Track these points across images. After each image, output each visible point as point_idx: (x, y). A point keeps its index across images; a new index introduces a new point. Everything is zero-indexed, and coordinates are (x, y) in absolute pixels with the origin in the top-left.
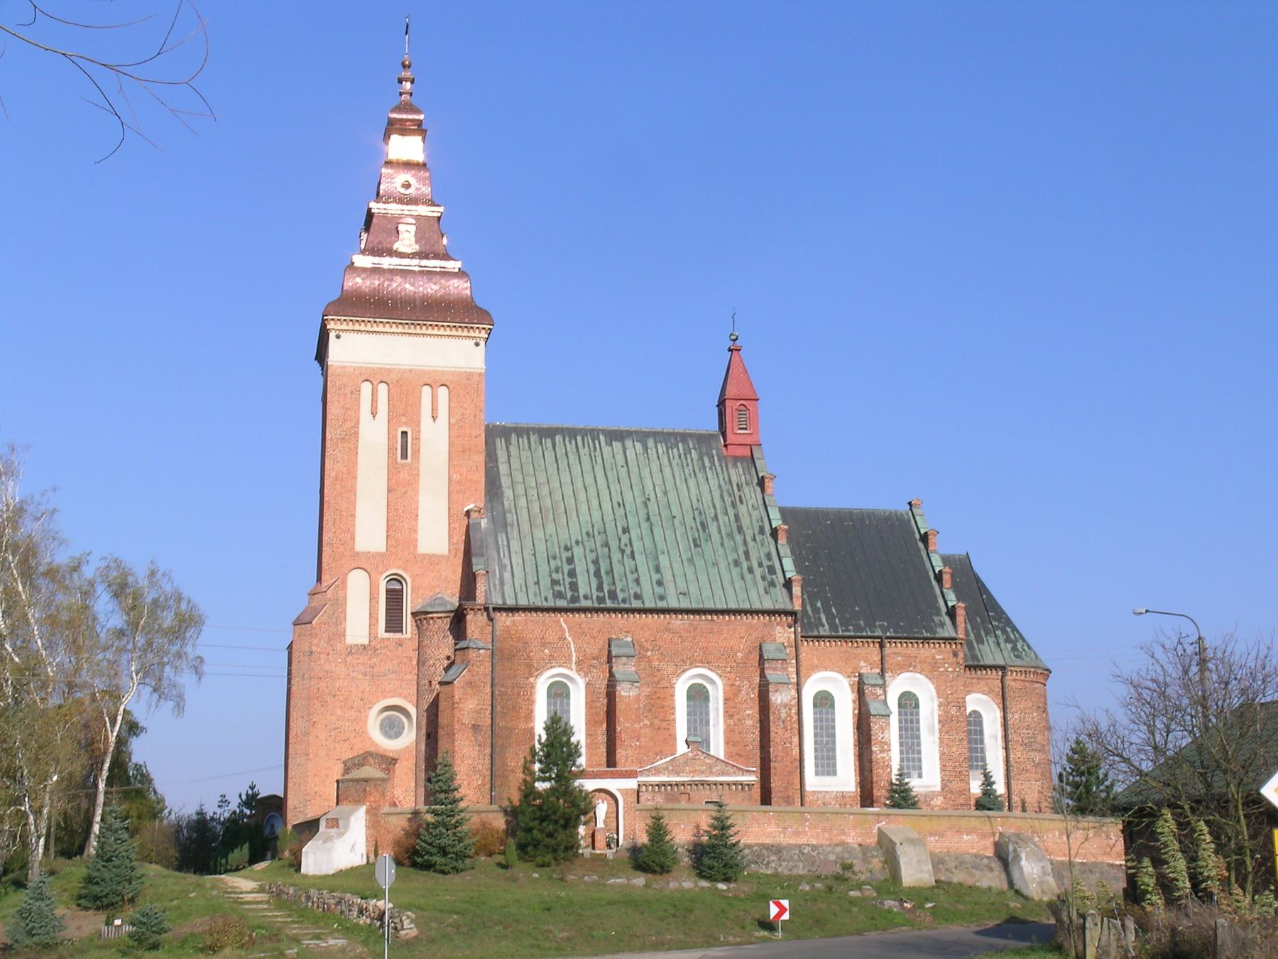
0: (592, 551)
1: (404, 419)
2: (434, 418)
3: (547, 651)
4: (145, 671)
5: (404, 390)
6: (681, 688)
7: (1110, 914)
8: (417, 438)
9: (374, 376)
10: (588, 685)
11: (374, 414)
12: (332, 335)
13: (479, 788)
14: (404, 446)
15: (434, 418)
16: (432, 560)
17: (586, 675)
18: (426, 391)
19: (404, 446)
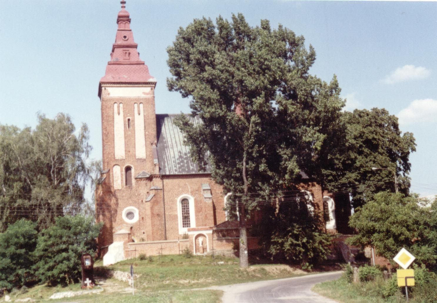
0: (174, 162)
1: (128, 115)
2: (139, 114)
3: (181, 189)
4: (237, 21)
5: (128, 104)
6: (179, 199)
7: (63, 199)
8: (133, 121)
9: (120, 101)
10: (195, 199)
11: (119, 114)
12: (103, 88)
13: (160, 235)
14: (129, 123)
15: (139, 114)
16: (143, 160)
17: (194, 196)
18: (136, 105)
19: (129, 123)
